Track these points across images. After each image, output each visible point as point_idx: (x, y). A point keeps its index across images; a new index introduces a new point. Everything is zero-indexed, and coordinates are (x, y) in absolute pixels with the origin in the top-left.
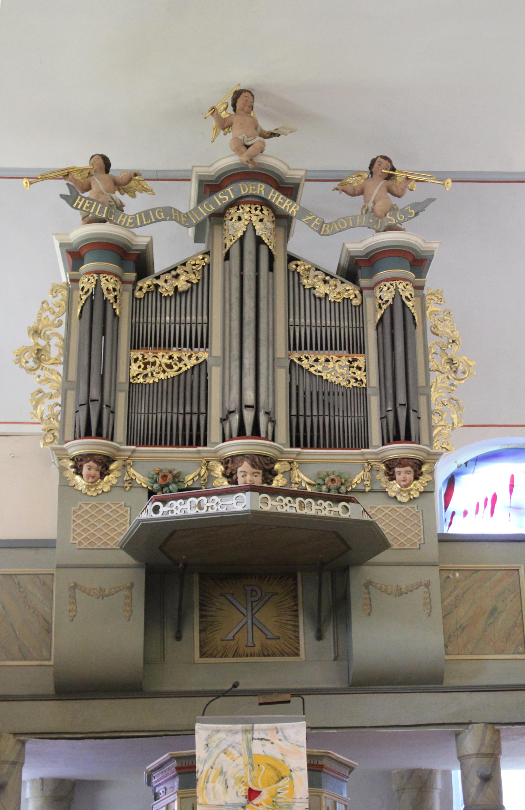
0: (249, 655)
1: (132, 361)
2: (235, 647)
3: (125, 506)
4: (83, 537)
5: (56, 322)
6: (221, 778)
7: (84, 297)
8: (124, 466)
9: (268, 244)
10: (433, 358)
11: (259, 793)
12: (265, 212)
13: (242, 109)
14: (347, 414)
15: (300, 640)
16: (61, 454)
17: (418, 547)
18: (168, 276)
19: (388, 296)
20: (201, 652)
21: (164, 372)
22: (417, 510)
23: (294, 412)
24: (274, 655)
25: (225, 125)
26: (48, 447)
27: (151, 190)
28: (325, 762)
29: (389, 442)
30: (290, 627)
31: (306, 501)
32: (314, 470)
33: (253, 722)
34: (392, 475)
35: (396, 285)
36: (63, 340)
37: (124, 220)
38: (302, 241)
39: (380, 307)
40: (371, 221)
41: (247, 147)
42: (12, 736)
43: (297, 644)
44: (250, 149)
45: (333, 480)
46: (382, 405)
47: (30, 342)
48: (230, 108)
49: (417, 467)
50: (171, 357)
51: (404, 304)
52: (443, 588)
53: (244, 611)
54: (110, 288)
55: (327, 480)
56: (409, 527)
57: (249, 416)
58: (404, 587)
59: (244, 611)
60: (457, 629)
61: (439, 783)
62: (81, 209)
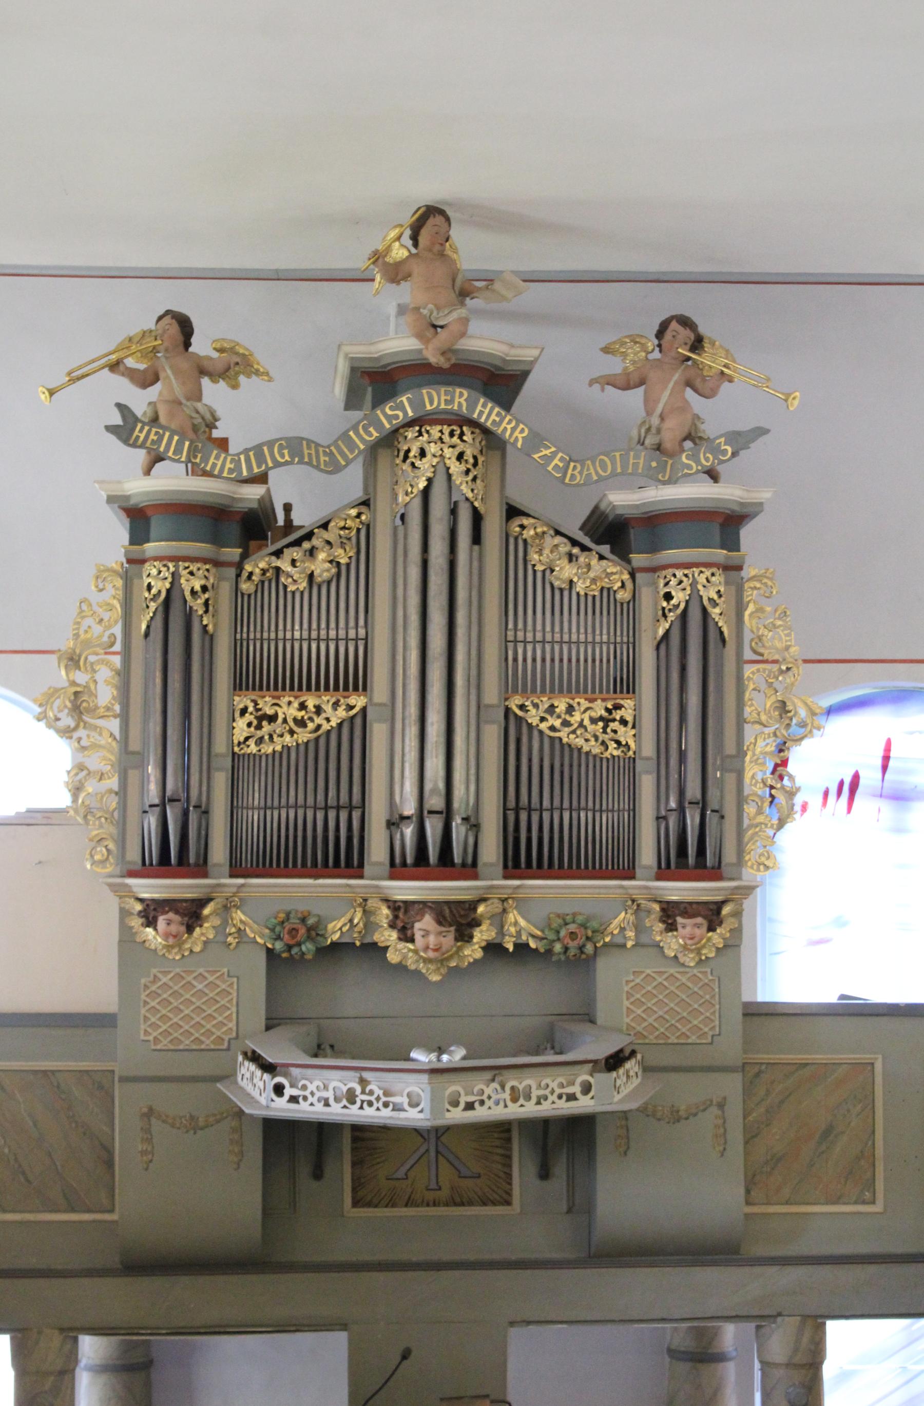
0: (431, 1203)
1: (237, 714)
2: (409, 1190)
3: (229, 976)
4: (161, 1030)
5: (105, 639)
7: (153, 606)
9: (472, 500)
10: (751, 700)
14: (608, 649)
15: (514, 1179)
17: (709, 1040)
19: (679, 597)
20: (353, 1198)
22: (711, 978)
24: (471, 1203)
27: (267, 374)
30: (498, 1158)
34: (671, 924)
35: (693, 575)
36: (118, 673)
37: (219, 463)
39: (664, 615)
40: (654, 464)
42: (56, 1332)
43: (508, 1187)
44: (443, 334)
45: (573, 935)
49: (712, 914)
50: (303, 706)
51: (705, 611)
54: (197, 588)
55: (563, 933)
56: (696, 1006)
57: (433, 829)
58: (683, 1107)
60: (766, 1163)
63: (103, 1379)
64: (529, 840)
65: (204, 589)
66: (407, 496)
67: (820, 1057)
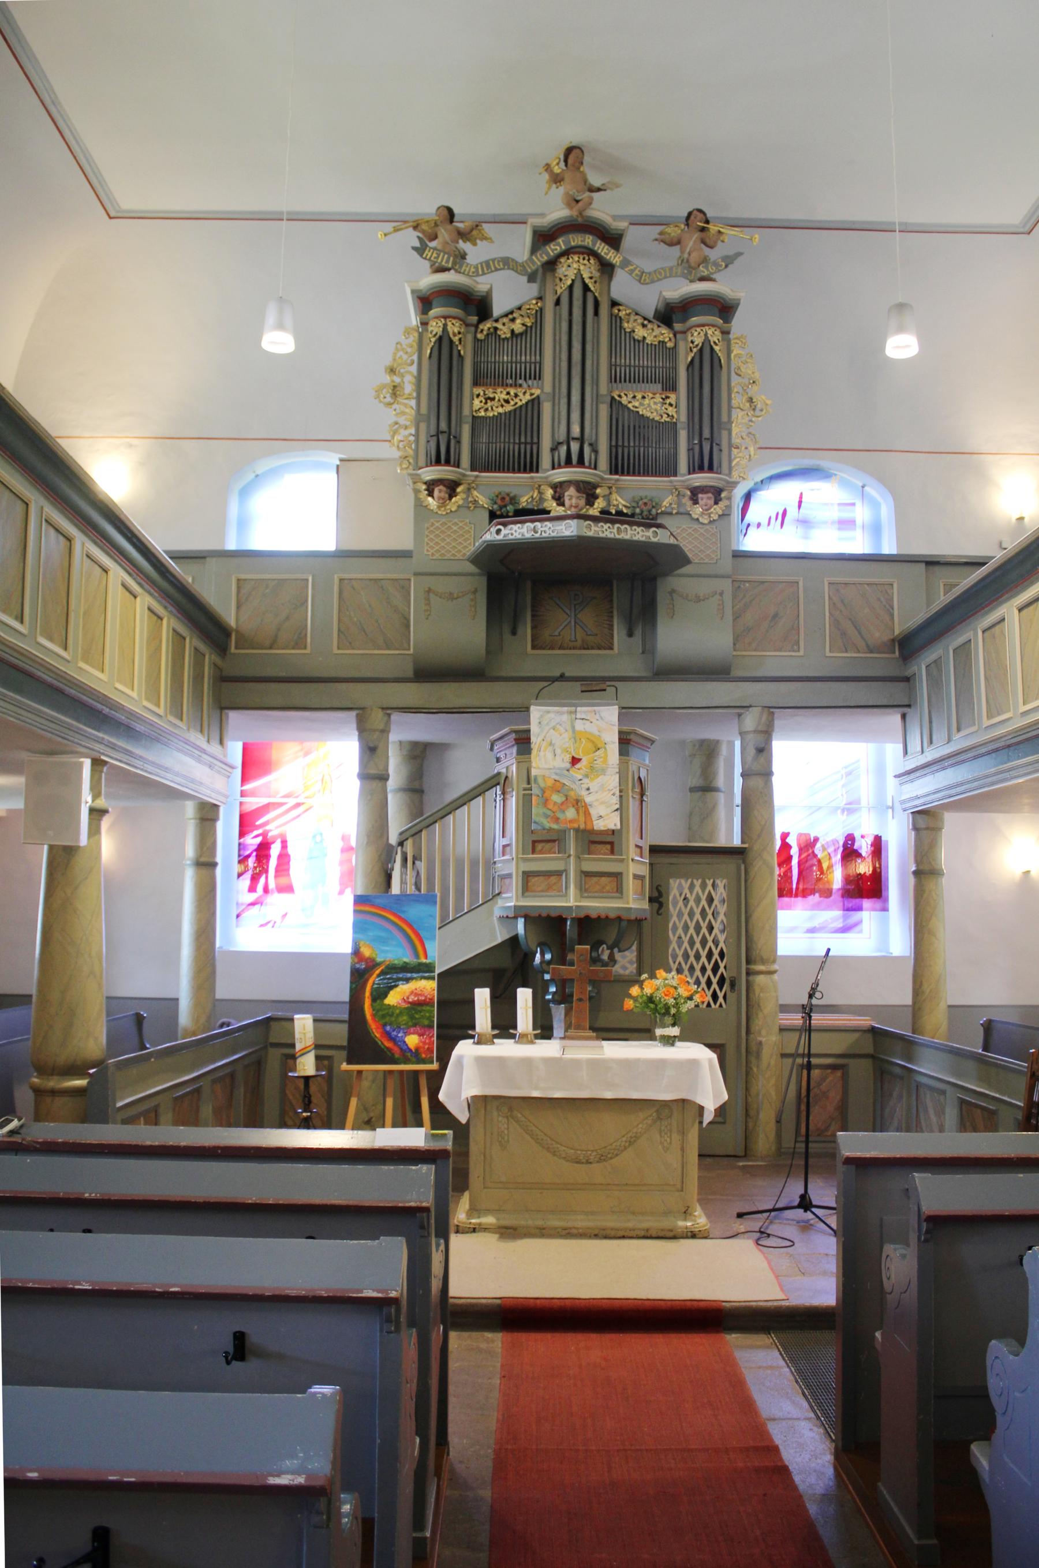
6: (551, 748)
7: (433, 340)
8: (469, 489)
11: (579, 760)
12: (592, 261)
13: (573, 165)
16: (416, 479)
18: (505, 320)
19: (699, 340)
21: (502, 406)
23: (614, 443)
24: (593, 648)
25: (557, 179)
26: (405, 472)
28: (632, 737)
29: (694, 472)
31: (623, 527)
33: (576, 706)
38: (622, 286)
41: (577, 201)
44: (580, 204)
45: (645, 504)
46: (690, 439)
47: (387, 379)
48: (562, 164)
49: (717, 493)
50: (508, 393)
51: (712, 349)
52: (734, 597)
53: (568, 611)
55: (641, 503)
57: (575, 447)
59: (568, 611)
61: (724, 750)
62: (430, 260)
63: (399, 795)
64: (623, 464)
65: (459, 333)
66: (562, 288)
67: (771, 578)
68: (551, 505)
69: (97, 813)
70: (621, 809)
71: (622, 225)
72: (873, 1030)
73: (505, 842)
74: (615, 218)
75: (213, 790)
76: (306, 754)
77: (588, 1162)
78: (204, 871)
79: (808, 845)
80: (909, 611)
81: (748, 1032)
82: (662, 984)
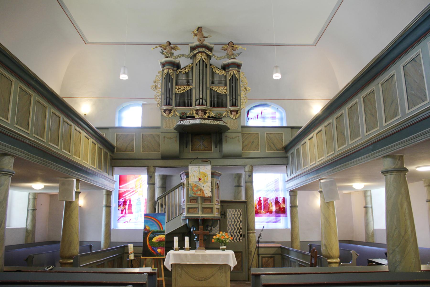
16: (161, 109)
19: (232, 74)
25: (196, 35)
32: (215, 112)
38: (213, 61)
49: (237, 112)
52: (242, 137)
57: (201, 100)
63: (160, 188)
68: (195, 115)
69: (78, 193)
70: (212, 192)
71: (212, 46)
72: (281, 247)
73: (183, 200)
74: (211, 43)
75: (110, 187)
76: (136, 178)
77: (202, 281)
78: (108, 208)
79: (266, 200)
80: (287, 139)
81: (248, 248)
82: (220, 235)
